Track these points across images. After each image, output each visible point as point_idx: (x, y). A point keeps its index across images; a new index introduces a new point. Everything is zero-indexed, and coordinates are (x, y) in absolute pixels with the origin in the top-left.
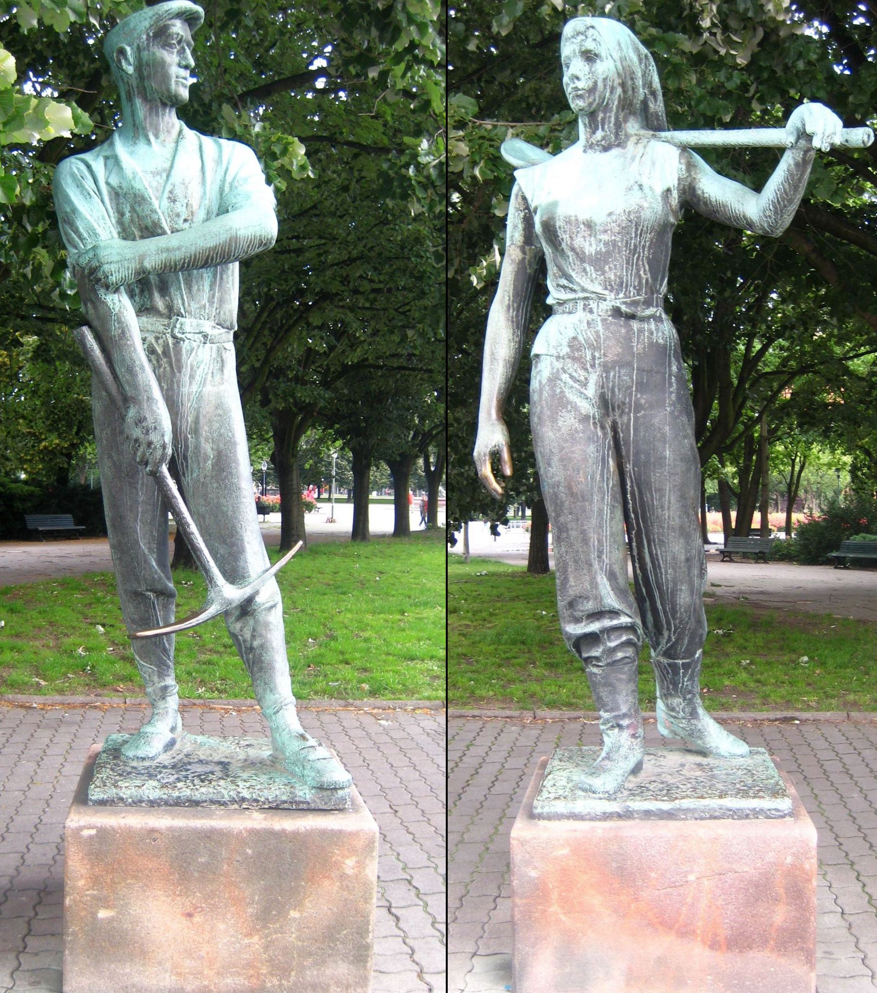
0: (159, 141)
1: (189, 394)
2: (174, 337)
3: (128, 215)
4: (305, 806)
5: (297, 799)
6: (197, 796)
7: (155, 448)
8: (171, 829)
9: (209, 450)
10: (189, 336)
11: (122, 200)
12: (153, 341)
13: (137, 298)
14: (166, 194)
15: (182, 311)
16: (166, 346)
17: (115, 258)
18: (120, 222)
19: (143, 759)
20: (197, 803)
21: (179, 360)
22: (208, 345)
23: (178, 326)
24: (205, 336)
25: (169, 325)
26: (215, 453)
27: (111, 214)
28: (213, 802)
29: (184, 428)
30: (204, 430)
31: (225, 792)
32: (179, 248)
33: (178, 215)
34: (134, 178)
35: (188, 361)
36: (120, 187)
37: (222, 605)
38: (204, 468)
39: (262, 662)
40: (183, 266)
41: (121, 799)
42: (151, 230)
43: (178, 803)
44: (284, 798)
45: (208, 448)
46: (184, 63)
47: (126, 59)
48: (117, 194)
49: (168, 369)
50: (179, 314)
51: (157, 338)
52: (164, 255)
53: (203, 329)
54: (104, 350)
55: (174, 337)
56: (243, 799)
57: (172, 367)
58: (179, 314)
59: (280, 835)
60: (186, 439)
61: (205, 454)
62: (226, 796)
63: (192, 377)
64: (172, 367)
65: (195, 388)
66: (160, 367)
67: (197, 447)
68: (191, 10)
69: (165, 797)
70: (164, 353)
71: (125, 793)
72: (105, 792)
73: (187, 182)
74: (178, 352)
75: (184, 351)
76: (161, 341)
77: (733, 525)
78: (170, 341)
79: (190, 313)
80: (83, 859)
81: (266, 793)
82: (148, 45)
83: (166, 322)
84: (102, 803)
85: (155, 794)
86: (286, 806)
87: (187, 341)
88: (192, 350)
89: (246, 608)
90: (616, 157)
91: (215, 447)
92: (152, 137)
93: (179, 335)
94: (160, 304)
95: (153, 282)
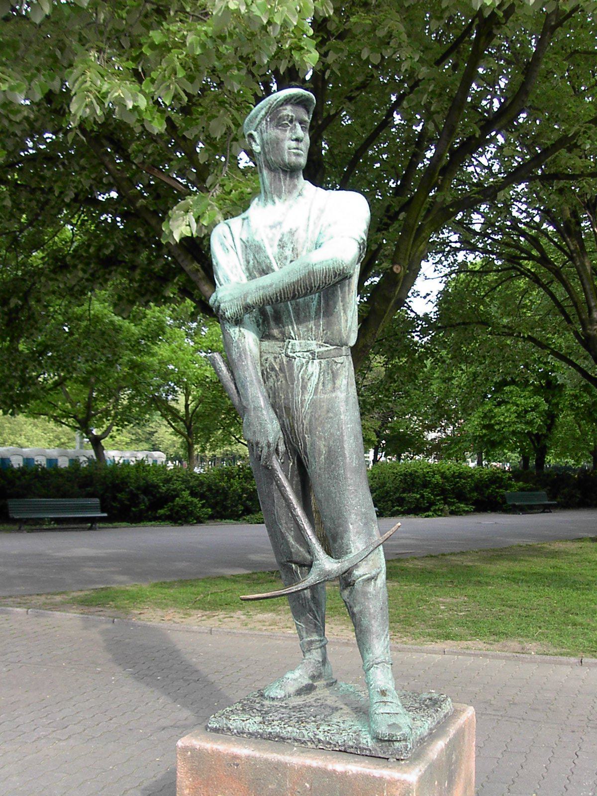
0: (282, 200)
1: (303, 401)
2: (287, 356)
3: (251, 262)
4: (368, 753)
5: (361, 745)
6: (284, 734)
7: (262, 448)
8: (248, 757)
9: (322, 447)
10: (299, 354)
11: (249, 251)
12: (273, 361)
13: (261, 327)
14: (277, 243)
15: (293, 334)
16: (282, 364)
17: (227, 299)
18: (248, 269)
19: (273, 699)
20: (283, 739)
21: (291, 375)
22: (316, 361)
23: (290, 347)
24: (313, 353)
25: (283, 346)
26: (327, 449)
27: (242, 263)
28: (296, 740)
29: (300, 429)
30: (319, 431)
31: (305, 733)
32: (271, 286)
33: (286, 258)
34: (256, 232)
35: (298, 374)
36: (248, 241)
37: (319, 575)
38: (319, 462)
39: (361, 626)
40: (277, 300)
41: (229, 729)
42: (265, 271)
43: (270, 737)
44: (351, 743)
45: (322, 445)
46: (294, 137)
47: (255, 142)
48: (246, 246)
49: (284, 382)
50: (290, 338)
51: (275, 358)
52: (261, 292)
53: (310, 348)
54: (231, 371)
55: (287, 356)
56: (319, 741)
57: (286, 380)
58: (290, 338)
59: (332, 774)
60: (304, 438)
61: (319, 450)
62: (306, 736)
63: (304, 388)
64: (286, 380)
65: (308, 397)
66: (278, 381)
67: (313, 444)
68: (302, 96)
69: (261, 731)
70: (280, 369)
71: (232, 725)
72: (218, 722)
73: (293, 231)
74: (291, 367)
75: (295, 367)
76: (278, 360)
77: (106, 515)
78: (285, 359)
79: (299, 336)
80: (187, 772)
81: (336, 738)
82: (267, 128)
83: (281, 344)
84: (216, 730)
85: (253, 728)
86: (352, 750)
87: (297, 359)
88: (302, 365)
89: (346, 580)
90: (257, 204)
91: (326, 444)
92: (276, 199)
93: (291, 355)
94: (276, 332)
95: (269, 313)
